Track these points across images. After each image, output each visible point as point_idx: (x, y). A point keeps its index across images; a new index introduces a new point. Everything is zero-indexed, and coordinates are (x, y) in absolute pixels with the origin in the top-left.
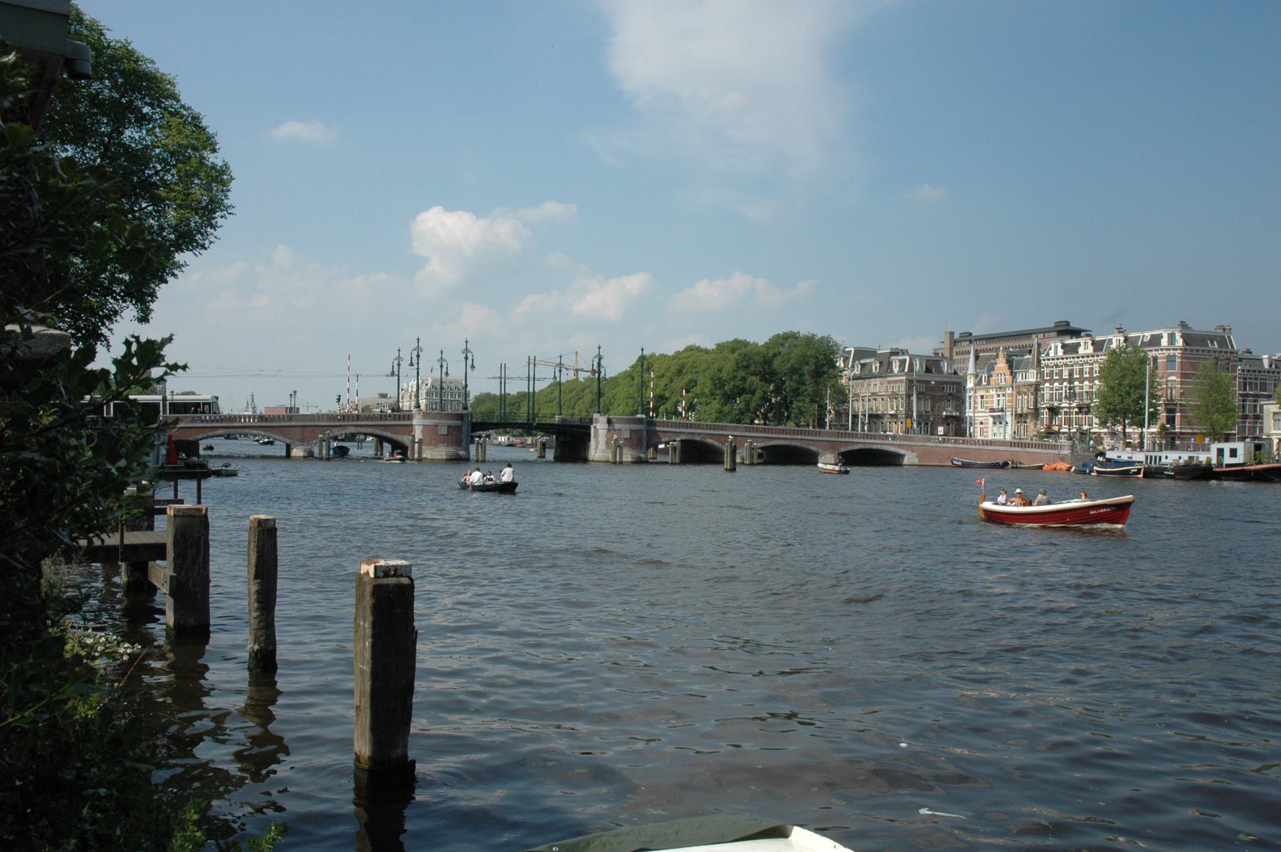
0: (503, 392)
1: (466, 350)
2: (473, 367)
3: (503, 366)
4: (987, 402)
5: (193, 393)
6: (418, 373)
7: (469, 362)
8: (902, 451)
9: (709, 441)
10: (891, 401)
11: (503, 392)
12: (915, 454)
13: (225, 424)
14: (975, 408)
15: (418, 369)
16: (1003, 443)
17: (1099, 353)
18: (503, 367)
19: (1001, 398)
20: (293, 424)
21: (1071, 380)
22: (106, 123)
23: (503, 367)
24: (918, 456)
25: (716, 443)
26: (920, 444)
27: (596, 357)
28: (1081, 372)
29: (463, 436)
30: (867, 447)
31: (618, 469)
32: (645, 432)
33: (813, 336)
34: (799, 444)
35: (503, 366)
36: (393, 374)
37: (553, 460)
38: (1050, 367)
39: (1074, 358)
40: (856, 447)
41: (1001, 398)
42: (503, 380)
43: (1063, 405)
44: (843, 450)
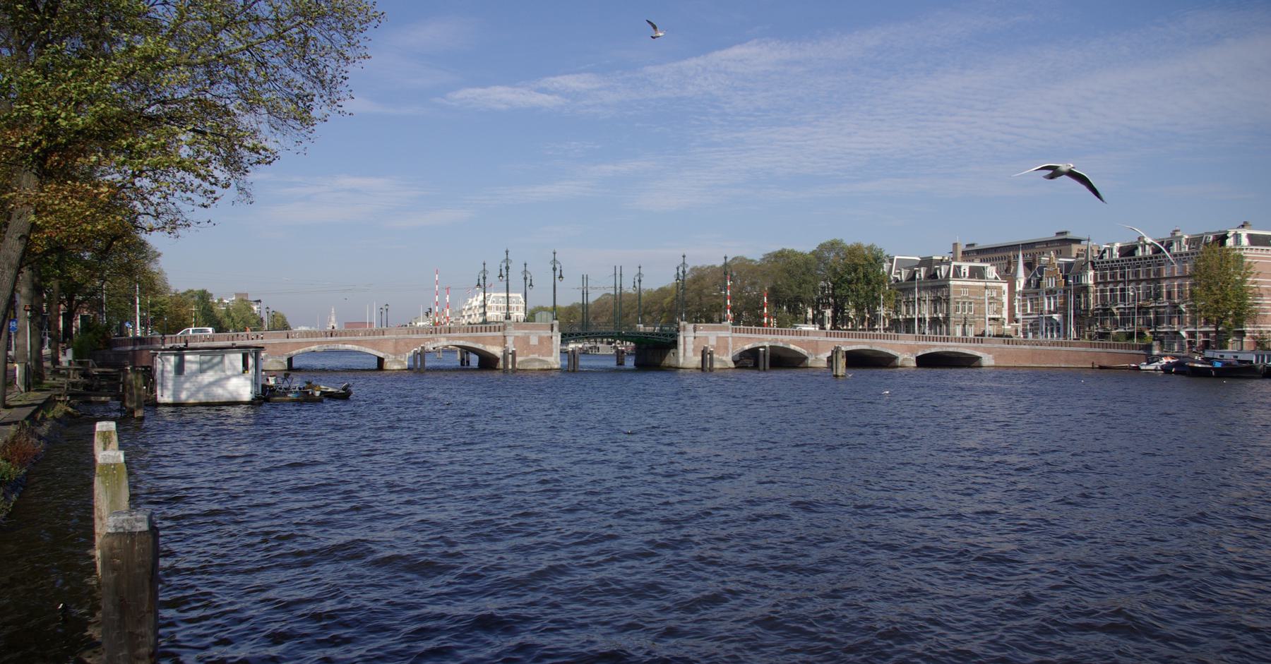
0: (585, 302)
2: (561, 276)
6: (507, 285)
7: (558, 273)
8: (978, 354)
9: (792, 347)
10: (1049, 299)
11: (585, 302)
15: (507, 280)
18: (585, 278)
22: (10, 469)
24: (995, 358)
29: (554, 346)
31: (464, 376)
37: (633, 367)
39: (1130, 260)
42: (585, 294)
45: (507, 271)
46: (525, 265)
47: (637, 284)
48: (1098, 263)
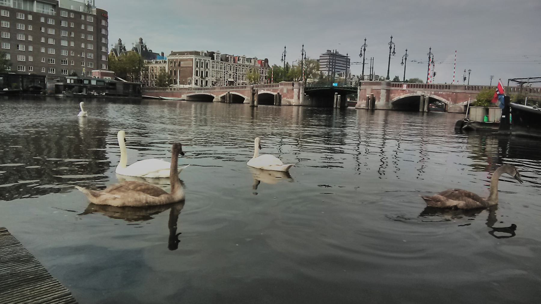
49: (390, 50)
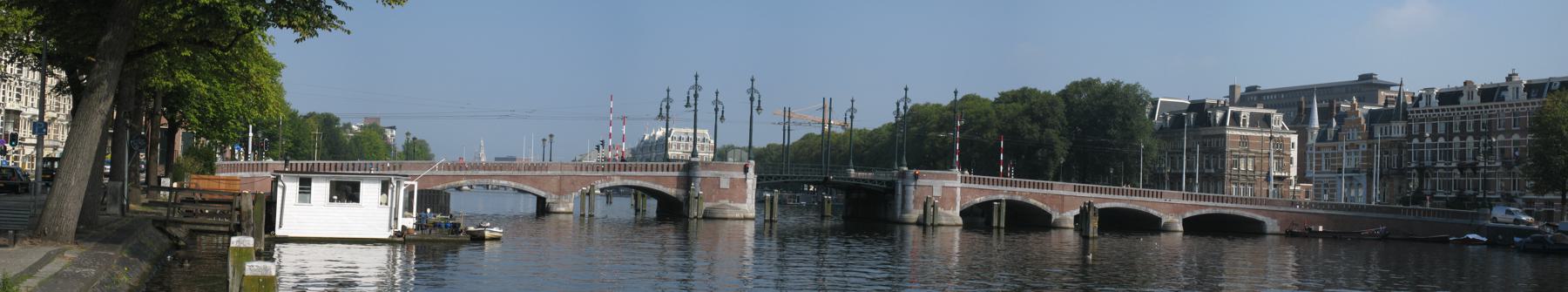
1: (717, 102)
2: (759, 108)
3: (787, 109)
4: (1334, 161)
5: (280, 227)
9: (1032, 201)
11: (786, 143)
12: (1275, 221)
13: (469, 173)
14: (1317, 168)
15: (696, 111)
16: (1370, 209)
17: (1489, 104)
18: (787, 113)
19: (1353, 157)
20: (549, 173)
21: (1449, 135)
23: (787, 113)
25: (1040, 204)
26: (1282, 209)
27: (849, 110)
28: (1463, 126)
30: (1218, 211)
32: (959, 190)
33: (1119, 84)
34: (1136, 207)
35: (787, 109)
36: (660, 116)
38: (1421, 120)
40: (1204, 212)
41: (1353, 157)
43: (1438, 165)
44: (1188, 215)
45: (696, 100)
46: (852, 101)
47: (849, 121)
48: (1412, 112)
49: (716, 113)
